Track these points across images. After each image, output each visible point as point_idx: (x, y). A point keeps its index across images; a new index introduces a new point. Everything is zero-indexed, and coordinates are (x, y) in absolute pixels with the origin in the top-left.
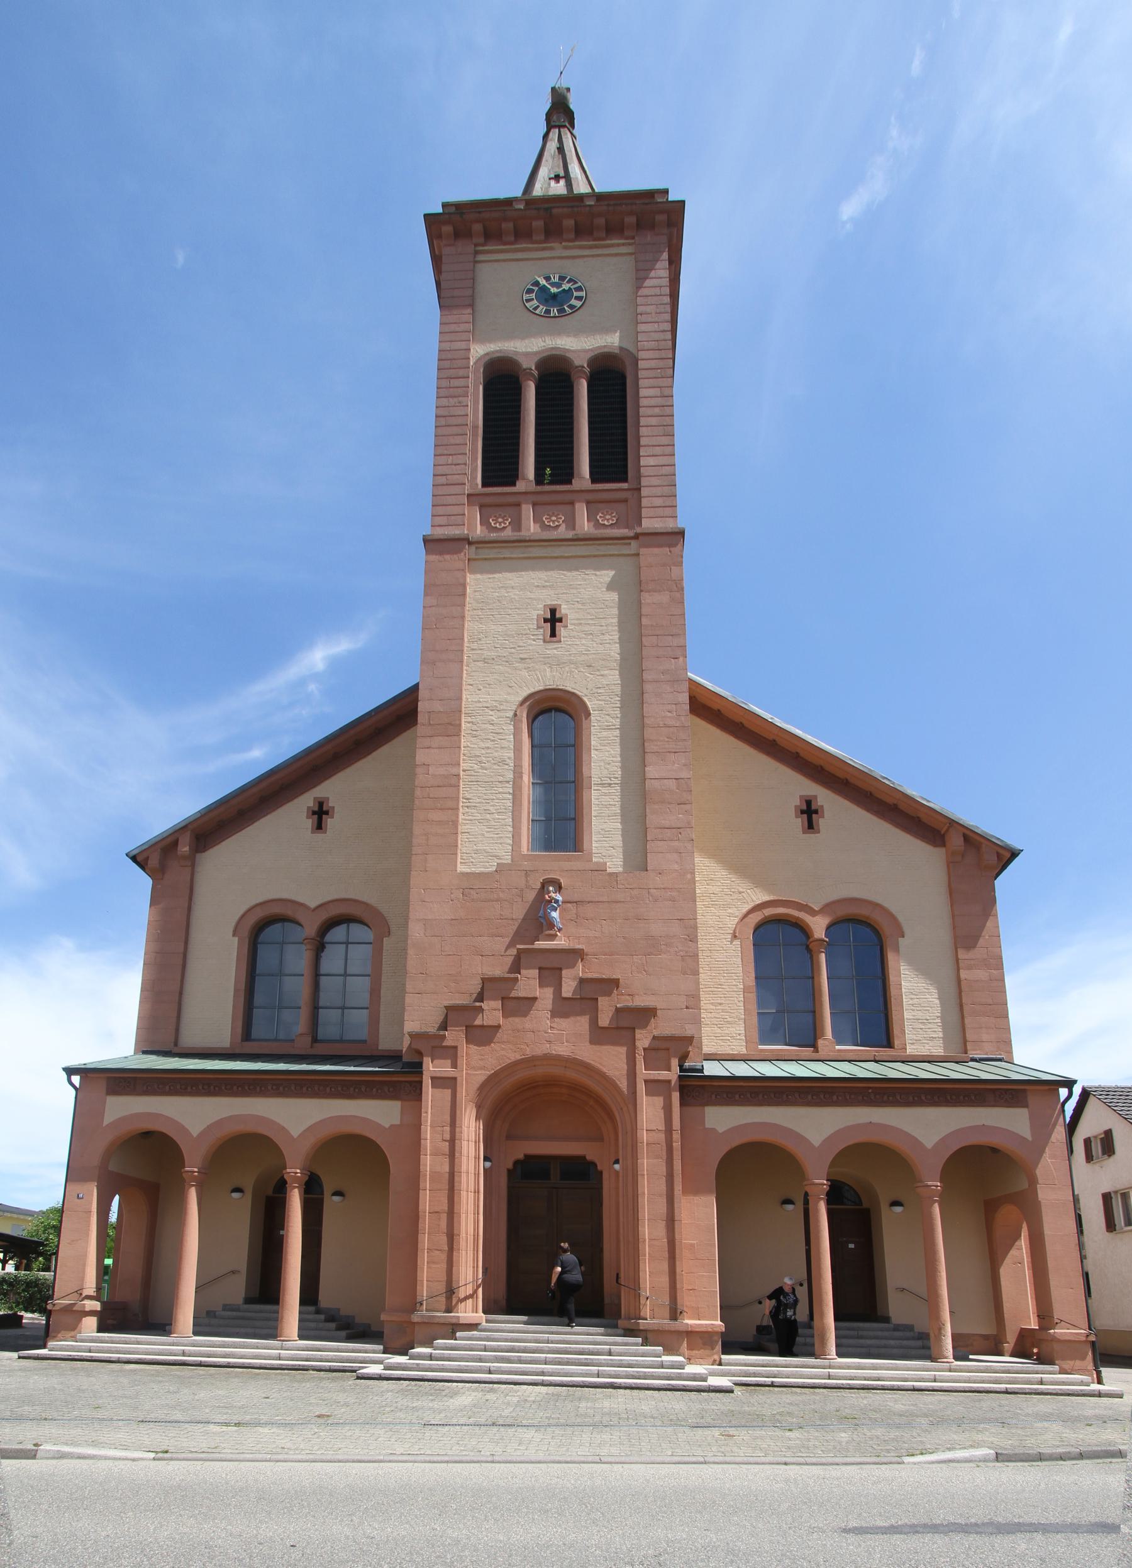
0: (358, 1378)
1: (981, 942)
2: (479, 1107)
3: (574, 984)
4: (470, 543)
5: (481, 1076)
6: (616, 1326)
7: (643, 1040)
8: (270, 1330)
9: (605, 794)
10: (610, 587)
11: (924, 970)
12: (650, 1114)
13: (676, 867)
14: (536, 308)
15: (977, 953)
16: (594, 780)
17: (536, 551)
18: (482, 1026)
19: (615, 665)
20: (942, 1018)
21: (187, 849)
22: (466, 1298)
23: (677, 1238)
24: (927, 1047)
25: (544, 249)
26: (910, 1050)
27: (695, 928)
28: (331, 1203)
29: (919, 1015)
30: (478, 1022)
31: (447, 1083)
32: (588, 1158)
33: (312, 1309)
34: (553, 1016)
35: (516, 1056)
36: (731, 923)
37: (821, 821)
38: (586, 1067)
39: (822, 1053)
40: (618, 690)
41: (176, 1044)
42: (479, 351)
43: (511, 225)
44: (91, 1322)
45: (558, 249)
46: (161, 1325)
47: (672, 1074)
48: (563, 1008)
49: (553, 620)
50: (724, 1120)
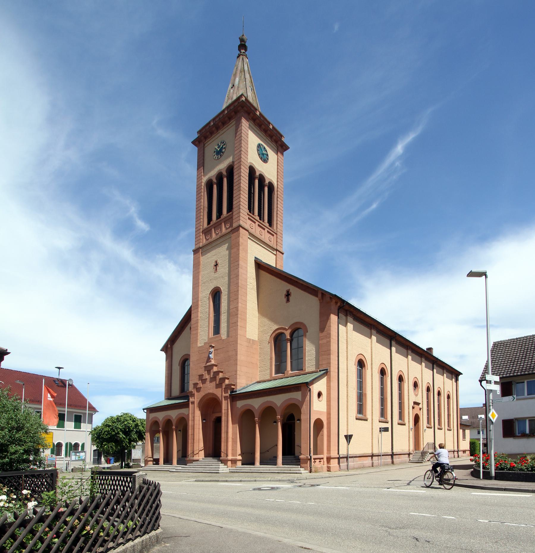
2: (199, 408)
4: (201, 248)
7: (224, 387)
11: (312, 342)
12: (225, 405)
15: (324, 333)
17: (214, 244)
31: (193, 403)
35: (204, 394)
36: (268, 338)
38: (204, 397)
41: (171, 396)
42: (205, 179)
44: (239, 464)
45: (221, 132)
46: (253, 463)
49: (216, 265)
50: (240, 404)
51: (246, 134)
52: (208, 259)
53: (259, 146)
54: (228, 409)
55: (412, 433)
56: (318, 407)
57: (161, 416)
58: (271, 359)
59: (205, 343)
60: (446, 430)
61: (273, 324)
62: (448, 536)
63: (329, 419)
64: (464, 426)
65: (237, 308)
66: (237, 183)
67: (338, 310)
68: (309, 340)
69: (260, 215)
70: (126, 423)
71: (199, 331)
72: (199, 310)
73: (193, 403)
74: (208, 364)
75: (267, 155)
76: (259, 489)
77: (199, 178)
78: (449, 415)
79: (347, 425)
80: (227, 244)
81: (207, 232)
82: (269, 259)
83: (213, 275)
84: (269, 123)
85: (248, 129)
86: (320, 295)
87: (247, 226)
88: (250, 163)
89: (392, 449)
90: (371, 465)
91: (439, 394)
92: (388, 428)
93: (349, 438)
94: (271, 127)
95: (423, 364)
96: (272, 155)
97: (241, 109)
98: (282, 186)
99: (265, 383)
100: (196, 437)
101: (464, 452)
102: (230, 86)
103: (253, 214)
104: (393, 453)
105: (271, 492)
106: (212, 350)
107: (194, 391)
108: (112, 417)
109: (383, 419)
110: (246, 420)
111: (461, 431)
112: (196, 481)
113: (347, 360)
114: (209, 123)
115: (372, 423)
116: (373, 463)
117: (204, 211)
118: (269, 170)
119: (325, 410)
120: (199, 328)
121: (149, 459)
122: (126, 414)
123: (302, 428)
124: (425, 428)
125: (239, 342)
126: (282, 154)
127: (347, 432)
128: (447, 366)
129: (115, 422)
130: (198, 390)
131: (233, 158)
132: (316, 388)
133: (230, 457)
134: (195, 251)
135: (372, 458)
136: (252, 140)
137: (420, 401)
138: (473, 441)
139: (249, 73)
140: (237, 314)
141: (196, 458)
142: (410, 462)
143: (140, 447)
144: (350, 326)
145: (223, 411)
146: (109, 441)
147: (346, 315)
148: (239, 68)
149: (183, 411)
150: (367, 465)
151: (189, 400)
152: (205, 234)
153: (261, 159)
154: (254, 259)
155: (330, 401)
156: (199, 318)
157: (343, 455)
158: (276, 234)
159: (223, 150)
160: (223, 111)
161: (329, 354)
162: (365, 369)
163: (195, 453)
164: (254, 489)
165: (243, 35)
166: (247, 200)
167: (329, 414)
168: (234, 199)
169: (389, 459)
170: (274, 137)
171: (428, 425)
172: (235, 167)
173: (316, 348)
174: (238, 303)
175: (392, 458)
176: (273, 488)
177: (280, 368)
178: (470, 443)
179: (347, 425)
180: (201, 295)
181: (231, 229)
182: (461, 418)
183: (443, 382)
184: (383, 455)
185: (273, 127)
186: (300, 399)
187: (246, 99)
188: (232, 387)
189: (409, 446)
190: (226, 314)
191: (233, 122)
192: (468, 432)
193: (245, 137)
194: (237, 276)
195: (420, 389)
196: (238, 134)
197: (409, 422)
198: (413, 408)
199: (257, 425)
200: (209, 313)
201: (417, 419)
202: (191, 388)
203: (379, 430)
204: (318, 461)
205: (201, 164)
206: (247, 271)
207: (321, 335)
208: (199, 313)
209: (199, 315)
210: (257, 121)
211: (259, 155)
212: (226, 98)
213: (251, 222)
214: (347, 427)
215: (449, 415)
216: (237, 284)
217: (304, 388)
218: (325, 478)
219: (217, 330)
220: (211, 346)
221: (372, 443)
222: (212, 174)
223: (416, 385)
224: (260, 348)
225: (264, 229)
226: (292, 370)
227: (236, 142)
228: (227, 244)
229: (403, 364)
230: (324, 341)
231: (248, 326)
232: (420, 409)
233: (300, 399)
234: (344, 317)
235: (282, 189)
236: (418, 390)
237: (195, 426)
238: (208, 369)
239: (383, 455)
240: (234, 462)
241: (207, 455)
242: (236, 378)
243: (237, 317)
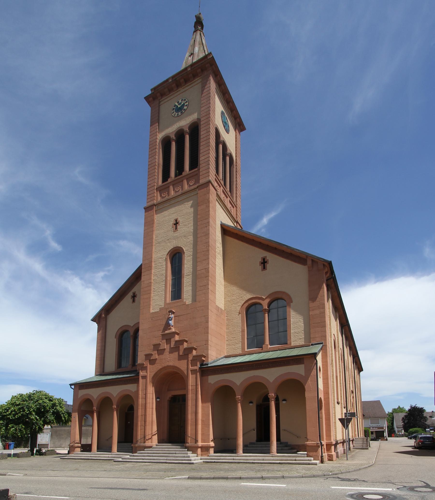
0: (114, 462)
1: (318, 299)
2: (153, 383)
3: (174, 343)
4: (155, 205)
5: (153, 374)
6: (183, 446)
7: (190, 357)
8: (268, 451)
9: (188, 278)
10: (191, 207)
12: (191, 380)
13: (204, 299)
14: (178, 114)
16: (185, 274)
17: (173, 202)
18: (153, 359)
19: (192, 234)
20: (304, 330)
21: (104, 315)
22: (149, 439)
23: (201, 417)
24: (298, 342)
25: (177, 92)
26: (293, 344)
27: (208, 318)
28: (283, 404)
29: (296, 330)
30: (152, 358)
31: (145, 377)
33: (279, 442)
34: (169, 353)
35: (161, 367)
36: (239, 308)
37: (268, 265)
39: (264, 349)
40: (192, 242)
41: (103, 372)
42: (160, 136)
43: (183, 80)
44: (212, 450)
45: (182, 90)
46: (233, 450)
47: (197, 367)
48: (172, 351)
49: (176, 223)
50: (213, 379)
52: (164, 219)
54: (196, 385)
57: (95, 394)
58: (243, 331)
59: (161, 309)
61: (244, 292)
65: (207, 270)
68: (295, 310)
70: (41, 402)
71: (152, 295)
72: (153, 273)
73: (145, 377)
74: (167, 332)
77: (153, 135)
80: (192, 202)
81: (161, 190)
86: (309, 262)
100: (149, 419)
102: (188, 54)
106: (172, 316)
107: (147, 364)
108: (21, 395)
110: (223, 399)
112: (189, 478)
117: (159, 167)
120: (152, 292)
121: (76, 445)
122: (40, 392)
125: (210, 307)
129: (26, 401)
130: (153, 362)
131: (199, 114)
133: (200, 444)
134: (147, 209)
135: (343, 445)
138: (366, 429)
140: (208, 276)
141: (148, 444)
143: (49, 431)
145: (190, 388)
146: (16, 422)
149: (130, 388)
152: (160, 191)
154: (220, 223)
156: (152, 281)
159: (185, 108)
163: (147, 438)
165: (200, 14)
172: (202, 123)
173: (304, 320)
177: (255, 341)
180: (154, 256)
181: (195, 186)
186: (303, 374)
188: (203, 359)
190: (191, 276)
191: (198, 80)
196: (205, 91)
199: (239, 405)
202: (141, 359)
205: (155, 119)
207: (312, 305)
208: (152, 276)
209: (152, 278)
216: (207, 243)
219: (177, 293)
222: (171, 130)
224: (228, 319)
226: (271, 344)
227: (202, 99)
228: (192, 202)
230: (317, 312)
233: (303, 374)
237: (148, 405)
238: (168, 338)
240: (205, 449)
241: (161, 441)
242: (207, 349)
243: (208, 280)
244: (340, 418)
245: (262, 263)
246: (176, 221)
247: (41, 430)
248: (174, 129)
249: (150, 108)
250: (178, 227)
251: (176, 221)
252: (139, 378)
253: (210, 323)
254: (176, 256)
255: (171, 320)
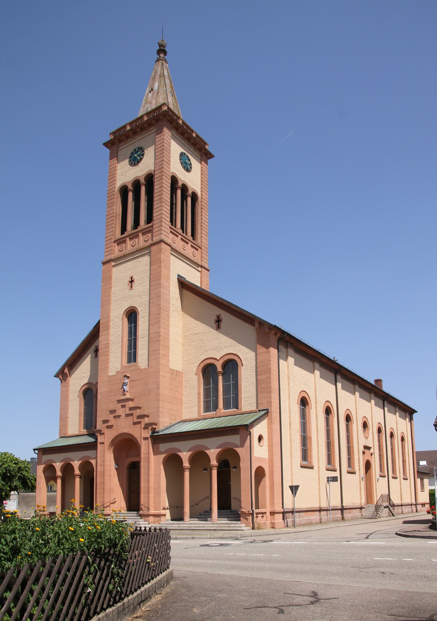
5: (110, 440)
12: (146, 447)
13: (155, 364)
16: (140, 337)
32: (241, 448)
35: (117, 434)
37: (222, 324)
49: (132, 281)
50: (164, 447)
51: (168, 143)
52: (120, 273)
53: (182, 154)
55: (363, 483)
56: (260, 453)
58: (199, 394)
59: (117, 372)
60: (402, 479)
62: (407, 570)
63: (271, 467)
64: (422, 474)
65: (158, 334)
66: (158, 194)
67: (278, 341)
69: (182, 228)
75: (191, 164)
76: (207, 545)
78: (404, 461)
79: (292, 474)
80: (90, 356)
82: (194, 277)
83: (127, 291)
84: (193, 131)
85: (170, 138)
86: (257, 325)
87: (169, 241)
88: (172, 172)
89: (342, 503)
90: (318, 521)
91: (392, 435)
92: (337, 477)
93: (294, 489)
94: (194, 135)
95: (373, 401)
96: (196, 164)
97: (163, 118)
98: (207, 196)
99: (192, 423)
101: (423, 505)
102: (148, 89)
103: (175, 227)
104: (342, 506)
105: (220, 548)
106: (127, 381)
109: (330, 466)
111: (418, 480)
113: (289, 399)
114: (125, 126)
115: (319, 471)
116: (321, 519)
118: (193, 179)
119: (267, 457)
123: (241, 477)
124: (378, 477)
125: (161, 373)
126: (206, 163)
127: (292, 482)
128: (400, 404)
132: (256, 431)
136: (176, 149)
137: (370, 445)
139: (169, 78)
142: (363, 517)
144: (291, 360)
145: (142, 456)
147: (287, 347)
148: (159, 73)
150: (314, 521)
151: (97, 439)
153: (184, 168)
154: (177, 277)
155: (272, 446)
157: (288, 509)
158: (200, 248)
160: (142, 117)
161: (270, 392)
162: (309, 408)
164: (201, 546)
166: (169, 212)
167: (271, 460)
168: (155, 211)
169: (338, 514)
170: (198, 146)
171: (381, 474)
172: (156, 176)
174: (159, 327)
175: (342, 514)
176: (221, 545)
177: (210, 404)
178: (430, 494)
179: (292, 474)
182: (418, 464)
183: (396, 422)
184: (332, 510)
185: (197, 135)
187: (169, 108)
188: (154, 426)
189: (361, 498)
192: (426, 481)
193: (168, 147)
194: (159, 296)
195: (370, 431)
197: (360, 470)
198: (364, 453)
200: (122, 336)
201: (368, 466)
202: (100, 426)
203: (326, 479)
204: (260, 516)
206: (169, 291)
210: (180, 130)
211: (182, 164)
212: (144, 101)
213: (174, 236)
214: (292, 477)
215: (404, 461)
217: (243, 430)
218: (272, 534)
219: (132, 356)
220: (125, 376)
221: (320, 495)
223: (365, 425)
225: (187, 243)
228: (90, 356)
229: (352, 402)
231: (171, 354)
232: (372, 454)
234: (284, 349)
235: (207, 200)
236: (368, 432)
237: (106, 472)
239: (332, 510)
242: (158, 416)
244: (290, 485)
245: (217, 321)
246: (132, 278)
247: (7, 496)
248: (131, 179)
249: (109, 150)
250: (134, 285)
251: (132, 278)
252: (97, 444)
253: (161, 390)
254: (132, 315)
255: (126, 385)
